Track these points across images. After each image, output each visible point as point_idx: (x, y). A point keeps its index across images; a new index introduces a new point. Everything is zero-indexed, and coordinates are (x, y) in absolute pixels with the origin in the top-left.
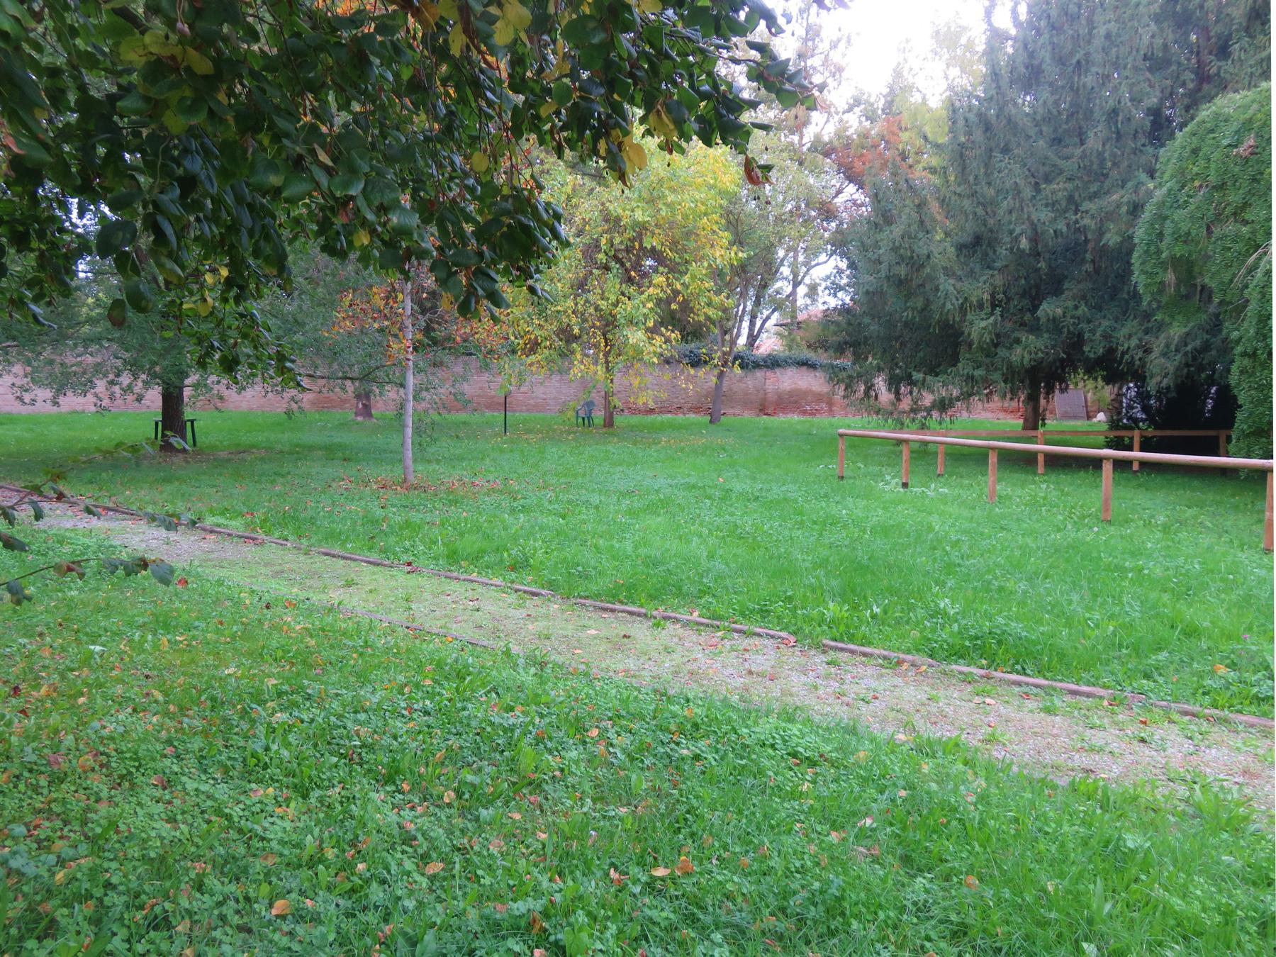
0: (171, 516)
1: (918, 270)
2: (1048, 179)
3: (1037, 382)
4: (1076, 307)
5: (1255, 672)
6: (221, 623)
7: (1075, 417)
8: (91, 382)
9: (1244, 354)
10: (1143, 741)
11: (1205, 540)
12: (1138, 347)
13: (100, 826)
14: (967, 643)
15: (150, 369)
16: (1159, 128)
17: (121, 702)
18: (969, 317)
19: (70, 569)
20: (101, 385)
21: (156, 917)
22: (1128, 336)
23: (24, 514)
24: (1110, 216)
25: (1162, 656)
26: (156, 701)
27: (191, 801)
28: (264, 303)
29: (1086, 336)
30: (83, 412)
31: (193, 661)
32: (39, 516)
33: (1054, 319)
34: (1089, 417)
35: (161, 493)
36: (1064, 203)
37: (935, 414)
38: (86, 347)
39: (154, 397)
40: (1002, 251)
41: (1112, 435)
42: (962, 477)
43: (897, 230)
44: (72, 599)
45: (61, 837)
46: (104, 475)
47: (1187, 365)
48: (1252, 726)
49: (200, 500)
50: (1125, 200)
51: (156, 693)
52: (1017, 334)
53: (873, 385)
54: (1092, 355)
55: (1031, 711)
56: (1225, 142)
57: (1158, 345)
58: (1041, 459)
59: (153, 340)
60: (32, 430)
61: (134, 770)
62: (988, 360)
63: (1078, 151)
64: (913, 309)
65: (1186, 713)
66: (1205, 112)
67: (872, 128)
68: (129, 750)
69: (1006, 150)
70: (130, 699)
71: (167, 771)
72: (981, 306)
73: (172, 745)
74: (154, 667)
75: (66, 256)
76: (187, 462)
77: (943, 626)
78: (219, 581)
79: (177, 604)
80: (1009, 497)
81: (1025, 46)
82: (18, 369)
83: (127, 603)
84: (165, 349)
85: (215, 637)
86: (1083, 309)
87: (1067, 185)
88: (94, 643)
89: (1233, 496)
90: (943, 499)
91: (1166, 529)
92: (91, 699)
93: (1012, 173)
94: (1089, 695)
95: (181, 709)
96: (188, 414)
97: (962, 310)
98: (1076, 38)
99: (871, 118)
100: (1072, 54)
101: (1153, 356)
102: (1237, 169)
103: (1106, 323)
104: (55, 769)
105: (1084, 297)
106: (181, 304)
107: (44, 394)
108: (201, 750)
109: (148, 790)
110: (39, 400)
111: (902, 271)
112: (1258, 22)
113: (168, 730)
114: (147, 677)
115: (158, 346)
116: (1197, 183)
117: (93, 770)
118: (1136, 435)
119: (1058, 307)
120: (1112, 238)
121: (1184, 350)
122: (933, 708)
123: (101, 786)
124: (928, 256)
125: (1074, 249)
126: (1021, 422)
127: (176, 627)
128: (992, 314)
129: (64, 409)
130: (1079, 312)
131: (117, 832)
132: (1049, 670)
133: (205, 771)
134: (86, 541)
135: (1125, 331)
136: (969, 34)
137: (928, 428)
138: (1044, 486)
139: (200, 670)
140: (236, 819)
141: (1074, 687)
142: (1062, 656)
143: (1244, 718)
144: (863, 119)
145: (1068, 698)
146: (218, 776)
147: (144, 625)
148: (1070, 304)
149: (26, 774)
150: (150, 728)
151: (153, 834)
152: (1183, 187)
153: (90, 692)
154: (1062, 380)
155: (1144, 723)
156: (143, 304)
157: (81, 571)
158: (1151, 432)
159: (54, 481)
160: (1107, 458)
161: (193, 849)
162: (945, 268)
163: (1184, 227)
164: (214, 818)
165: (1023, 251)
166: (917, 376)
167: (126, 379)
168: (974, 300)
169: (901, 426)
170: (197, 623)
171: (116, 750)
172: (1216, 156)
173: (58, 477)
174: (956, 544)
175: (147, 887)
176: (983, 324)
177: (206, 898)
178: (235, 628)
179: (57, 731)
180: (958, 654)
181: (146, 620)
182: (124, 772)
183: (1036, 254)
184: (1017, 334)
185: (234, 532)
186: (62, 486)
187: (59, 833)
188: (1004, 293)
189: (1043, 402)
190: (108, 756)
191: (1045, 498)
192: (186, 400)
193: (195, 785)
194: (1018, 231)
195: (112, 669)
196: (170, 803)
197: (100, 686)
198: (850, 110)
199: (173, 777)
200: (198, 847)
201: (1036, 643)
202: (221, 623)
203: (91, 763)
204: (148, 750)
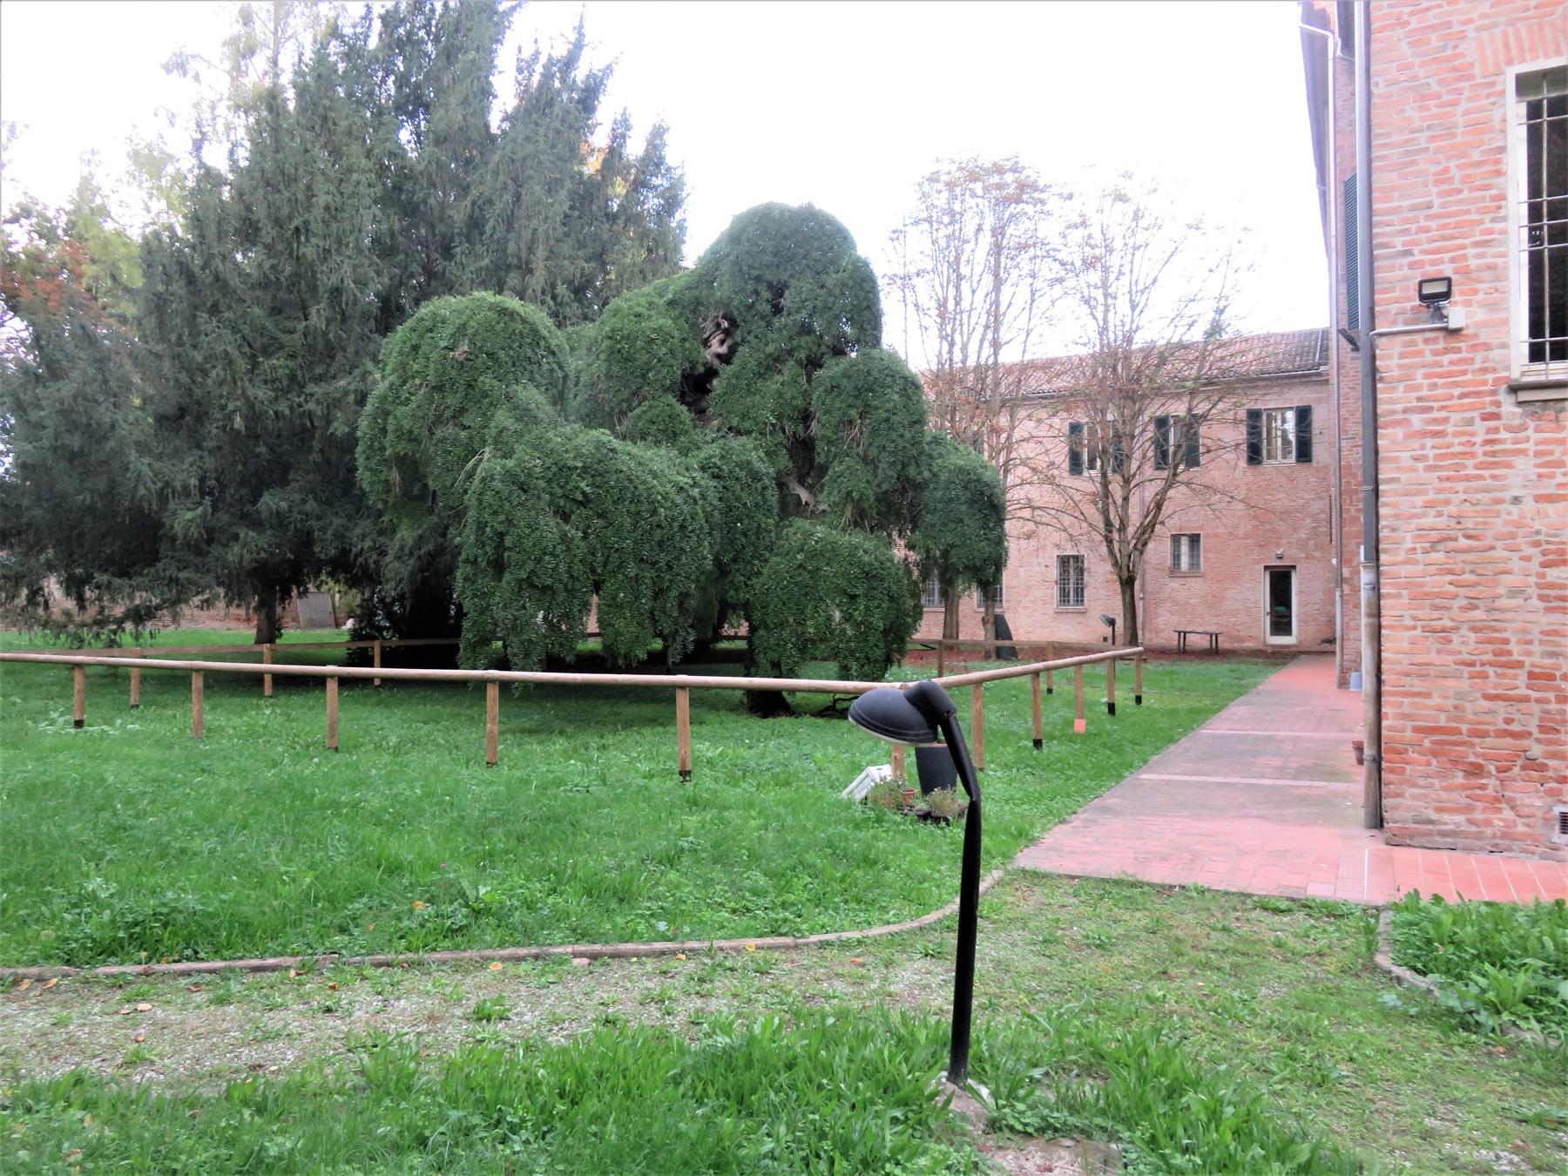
1: (98, 442)
2: (266, 352)
3: (269, 587)
4: (304, 502)
5: (451, 903)
7: (323, 625)
9: (467, 561)
10: (329, 1010)
11: (433, 760)
12: (372, 549)
14: (121, 934)
16: (389, 314)
18: (172, 505)
22: (361, 537)
24: (336, 403)
25: (359, 905)
28: (1381, 84)
29: (316, 534)
33: (278, 513)
34: (338, 625)
36: (285, 382)
37: (129, 626)
40: (213, 429)
41: (355, 646)
42: (164, 707)
43: (66, 389)
47: (422, 571)
48: (445, 962)
50: (352, 387)
52: (235, 529)
53: (41, 589)
54: (323, 556)
55: (198, 1007)
56: (443, 344)
57: (393, 548)
58: (268, 679)
62: (198, 560)
63: (301, 326)
64: (93, 491)
65: (380, 965)
66: (425, 310)
67: (48, 250)
69: (214, 310)
72: (186, 491)
77: (89, 916)
80: (221, 728)
81: (241, 195)
86: (311, 505)
87: (288, 362)
89: (470, 707)
90: (131, 739)
91: (396, 751)
93: (219, 338)
94: (274, 969)
97: (163, 497)
98: (294, 201)
99: (48, 234)
100: (290, 218)
101: (388, 559)
102: (453, 373)
103: (337, 521)
105: (313, 491)
111: (76, 442)
112: (476, 231)
116: (417, 381)
118: (377, 645)
119: (282, 499)
120: (339, 428)
121: (417, 553)
122: (59, 1036)
124: (113, 427)
125: (302, 433)
126: (254, 632)
128: (200, 504)
130: (308, 508)
132: (229, 946)
135: (358, 531)
136: (177, 165)
137: (120, 646)
138: (268, 712)
141: (256, 962)
142: (246, 926)
143: (438, 956)
144: (35, 236)
145: (249, 979)
148: (297, 497)
152: (405, 382)
154: (300, 583)
155: (333, 988)
158: (395, 641)
160: (332, 676)
162: (138, 443)
163: (407, 424)
165: (239, 432)
166: (102, 578)
168: (178, 485)
169: (79, 643)
172: (434, 356)
174: (130, 801)
176: (189, 515)
180: (107, 950)
183: (253, 434)
184: (235, 529)
188: (217, 479)
189: (279, 610)
191: (265, 727)
194: (231, 407)
198: (15, 220)
201: (210, 916)
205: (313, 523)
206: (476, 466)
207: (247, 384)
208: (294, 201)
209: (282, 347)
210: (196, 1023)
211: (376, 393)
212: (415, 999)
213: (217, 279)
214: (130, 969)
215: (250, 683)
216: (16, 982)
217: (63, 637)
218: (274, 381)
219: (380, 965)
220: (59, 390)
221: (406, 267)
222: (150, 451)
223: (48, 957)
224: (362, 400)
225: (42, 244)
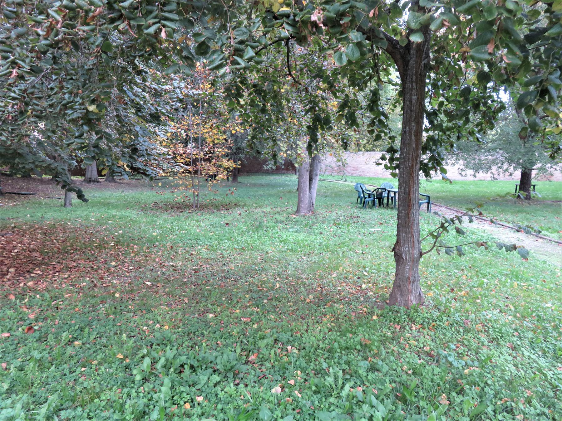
0: (529, 227)
6: (544, 281)
8: (490, 167)
13: (484, 357)
17: (496, 306)
19: (482, 245)
20: (494, 169)
21: (507, 407)
23: (466, 219)
26: (510, 310)
30: (484, 180)
31: (529, 296)
32: (471, 221)
35: (517, 217)
38: (489, 152)
39: (518, 174)
45: (467, 355)
49: (536, 222)
51: (511, 306)
59: (520, 148)
60: (463, 187)
61: (499, 337)
68: (497, 328)
70: (499, 306)
71: (515, 343)
73: (517, 332)
74: (510, 295)
75: (494, 112)
76: (530, 204)
78: (544, 261)
79: (522, 268)
82: (461, 162)
83: (499, 264)
84: (525, 152)
85: (541, 287)
88: (484, 278)
92: (482, 301)
95: (523, 317)
96: (533, 182)
104: (466, 326)
106: (545, 129)
107: (470, 172)
108: (532, 338)
109: (505, 348)
113: (516, 325)
114: (507, 298)
115: (523, 151)
117: (482, 331)
123: (485, 340)
127: (521, 279)
129: (476, 179)
131: (491, 362)
133: (533, 349)
134: (483, 234)
139: (532, 301)
140: (549, 378)
146: (540, 353)
147: (507, 274)
149: (455, 325)
150: (507, 321)
151: (507, 369)
153: (482, 298)
156: (537, 128)
157: (487, 246)
159: (478, 207)
161: (526, 383)
164: (537, 373)
167: (506, 166)
170: (532, 279)
173: (480, 205)
177: (532, 409)
178: (552, 286)
181: (508, 273)
185: (553, 239)
186: (481, 210)
187: (466, 353)
190: (489, 328)
192: (533, 176)
193: (528, 354)
195: (491, 291)
196: (515, 357)
197: (486, 297)
199: (517, 346)
200: (528, 383)
202: (544, 281)
203: (481, 328)
204: (506, 330)
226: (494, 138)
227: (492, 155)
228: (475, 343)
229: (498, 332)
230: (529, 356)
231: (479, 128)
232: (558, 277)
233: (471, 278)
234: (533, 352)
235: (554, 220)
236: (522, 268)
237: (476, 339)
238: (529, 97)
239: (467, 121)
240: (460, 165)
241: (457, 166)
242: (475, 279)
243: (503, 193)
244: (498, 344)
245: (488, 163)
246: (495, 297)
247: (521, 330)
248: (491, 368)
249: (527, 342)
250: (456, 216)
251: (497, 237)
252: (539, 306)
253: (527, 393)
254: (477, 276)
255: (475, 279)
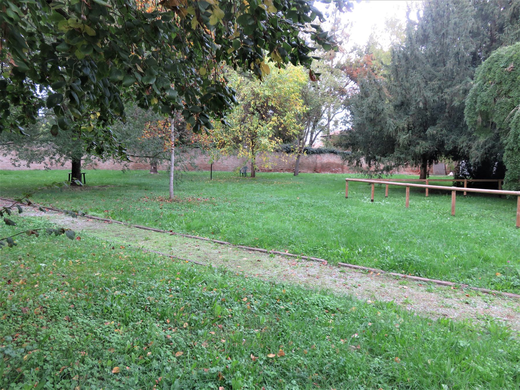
0: (75, 212)
1: (378, 115)
2: (431, 80)
3: (426, 160)
4: (442, 130)
5: (512, 276)
6: (94, 255)
7: (441, 174)
8: (43, 158)
9: (509, 149)
10: (467, 303)
11: (493, 223)
12: (466, 146)
13: (43, 337)
14: (397, 264)
15: (67, 153)
16: (475, 60)
17: (52, 286)
18: (399, 134)
19: (33, 233)
20: (47, 159)
22: (462, 142)
23: (14, 210)
24: (455, 94)
25: (475, 269)
26: (67, 286)
27: (80, 327)
28: (114, 127)
30: (40, 170)
31: (82, 270)
32: (20, 211)
33: (433, 135)
35: (71, 202)
36: (437, 89)
37: (385, 172)
38: (41, 144)
39: (69, 164)
40: (412, 108)
43: (370, 99)
44: (33, 245)
45: (26, 341)
46: (47, 195)
47: (486, 153)
48: (511, 297)
49: (86, 205)
50: (462, 88)
51: (67, 283)
52: (418, 141)
53: (360, 161)
54: (448, 149)
55: (422, 291)
56: (502, 66)
57: (474, 145)
58: (427, 190)
61: (57, 314)
62: (406, 151)
63: (443, 69)
65: (484, 292)
66: (494, 54)
68: (55, 306)
69: (414, 68)
70: (56, 285)
71: (71, 314)
72: (403, 129)
73: (73, 304)
74: (66, 273)
76: (82, 190)
77: (387, 257)
78: (93, 238)
79: (76, 247)
82: (13, 152)
84: (73, 145)
85: (91, 260)
86: (444, 131)
88: (42, 263)
89: (504, 205)
90: (388, 206)
91: (477, 218)
93: (416, 77)
94: (445, 285)
96: (82, 171)
98: (443, 24)
99: (360, 55)
100: (441, 30)
101: (472, 150)
102: (506, 76)
103: (453, 137)
105: (445, 126)
106: (81, 127)
107: (24, 162)
108: (85, 306)
109: (62, 322)
110: (22, 165)
111: (372, 116)
113: (71, 298)
114: (63, 276)
116: (490, 82)
117: (40, 314)
119: (434, 130)
121: (484, 147)
122: (383, 290)
123: (43, 321)
124: (383, 110)
126: (419, 176)
127: (75, 256)
128: (408, 133)
129: (32, 168)
130: (443, 132)
131: (50, 339)
132: (429, 275)
133: (86, 315)
134: (40, 221)
136: (400, 22)
137: (382, 178)
138: (428, 201)
142: (435, 269)
144: (357, 55)
145: (437, 286)
146: (91, 316)
147: (63, 255)
148: (439, 129)
149: (13, 316)
151: (64, 340)
152: (485, 83)
153: (40, 282)
154: (436, 159)
155: (468, 296)
158: (471, 180)
159: (27, 197)
161: (80, 346)
162: (389, 115)
163: (485, 99)
164: (89, 334)
165: (421, 108)
166: (378, 157)
167: (57, 157)
168: (401, 127)
170: (84, 255)
171: (50, 306)
172: (498, 71)
173: (28, 196)
174: (393, 224)
175: (61, 362)
176: (404, 137)
177: (85, 366)
178: (100, 257)
179: (26, 298)
180: (393, 268)
181: (63, 253)
182: (53, 315)
183: (426, 109)
184: (418, 141)
185: (100, 218)
186: (30, 200)
187: (25, 340)
189: (428, 168)
190: (47, 308)
191: (428, 206)
192: (82, 165)
193: (82, 320)
194: (419, 100)
196: (71, 327)
197: (44, 280)
198: (352, 52)
199: (73, 317)
200: (82, 345)
202: (94, 255)
203: (39, 311)
204: (63, 306)
205: (444, 138)
206: (515, 112)
207: (424, 91)
208: (443, 24)
209: (436, 77)
210: (422, 296)
211: (473, 88)
212: (500, 307)
213: (416, 57)
214: (399, 274)
215: (421, 191)
216: (369, 272)
217: (366, 175)
218: (433, 90)
219: (484, 292)
220: (368, 100)
221: (483, 40)
222: (393, 117)
223: (377, 267)
224: (466, 92)
225: (359, 57)
226: (45, 130)
227: (43, 147)
228: (34, 327)
229: (56, 310)
230: (82, 322)
231: (22, 121)
232: (105, 249)
233: (29, 265)
234: (86, 317)
235: (101, 202)
236: (76, 247)
237: (35, 323)
238: (57, 99)
239: (7, 113)
240: (13, 155)
241: (9, 157)
242: (33, 265)
243: (49, 183)
244: (56, 320)
245: (40, 154)
246: (53, 278)
247: (75, 302)
248: (49, 345)
249: (81, 311)
250: (4, 208)
251: (53, 222)
252: (90, 277)
253: (81, 354)
254: (35, 262)
255: (33, 265)
